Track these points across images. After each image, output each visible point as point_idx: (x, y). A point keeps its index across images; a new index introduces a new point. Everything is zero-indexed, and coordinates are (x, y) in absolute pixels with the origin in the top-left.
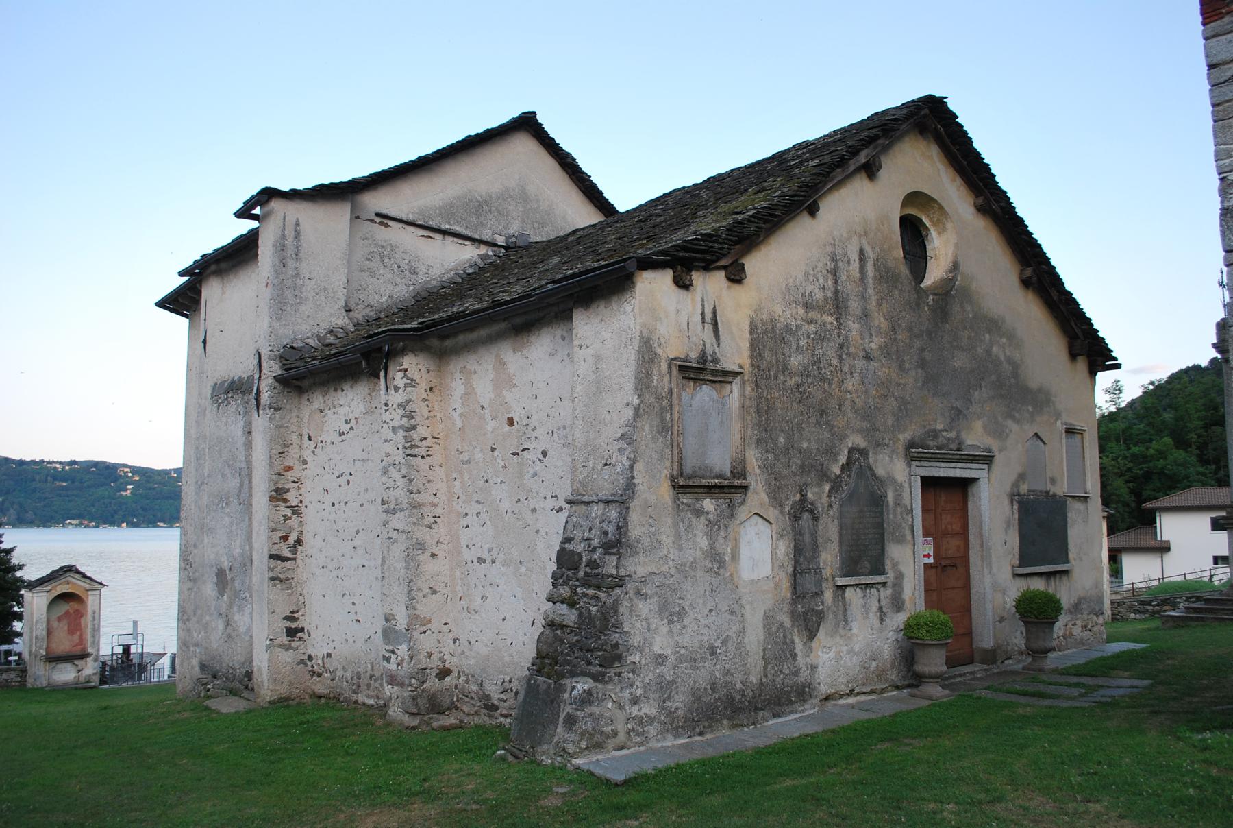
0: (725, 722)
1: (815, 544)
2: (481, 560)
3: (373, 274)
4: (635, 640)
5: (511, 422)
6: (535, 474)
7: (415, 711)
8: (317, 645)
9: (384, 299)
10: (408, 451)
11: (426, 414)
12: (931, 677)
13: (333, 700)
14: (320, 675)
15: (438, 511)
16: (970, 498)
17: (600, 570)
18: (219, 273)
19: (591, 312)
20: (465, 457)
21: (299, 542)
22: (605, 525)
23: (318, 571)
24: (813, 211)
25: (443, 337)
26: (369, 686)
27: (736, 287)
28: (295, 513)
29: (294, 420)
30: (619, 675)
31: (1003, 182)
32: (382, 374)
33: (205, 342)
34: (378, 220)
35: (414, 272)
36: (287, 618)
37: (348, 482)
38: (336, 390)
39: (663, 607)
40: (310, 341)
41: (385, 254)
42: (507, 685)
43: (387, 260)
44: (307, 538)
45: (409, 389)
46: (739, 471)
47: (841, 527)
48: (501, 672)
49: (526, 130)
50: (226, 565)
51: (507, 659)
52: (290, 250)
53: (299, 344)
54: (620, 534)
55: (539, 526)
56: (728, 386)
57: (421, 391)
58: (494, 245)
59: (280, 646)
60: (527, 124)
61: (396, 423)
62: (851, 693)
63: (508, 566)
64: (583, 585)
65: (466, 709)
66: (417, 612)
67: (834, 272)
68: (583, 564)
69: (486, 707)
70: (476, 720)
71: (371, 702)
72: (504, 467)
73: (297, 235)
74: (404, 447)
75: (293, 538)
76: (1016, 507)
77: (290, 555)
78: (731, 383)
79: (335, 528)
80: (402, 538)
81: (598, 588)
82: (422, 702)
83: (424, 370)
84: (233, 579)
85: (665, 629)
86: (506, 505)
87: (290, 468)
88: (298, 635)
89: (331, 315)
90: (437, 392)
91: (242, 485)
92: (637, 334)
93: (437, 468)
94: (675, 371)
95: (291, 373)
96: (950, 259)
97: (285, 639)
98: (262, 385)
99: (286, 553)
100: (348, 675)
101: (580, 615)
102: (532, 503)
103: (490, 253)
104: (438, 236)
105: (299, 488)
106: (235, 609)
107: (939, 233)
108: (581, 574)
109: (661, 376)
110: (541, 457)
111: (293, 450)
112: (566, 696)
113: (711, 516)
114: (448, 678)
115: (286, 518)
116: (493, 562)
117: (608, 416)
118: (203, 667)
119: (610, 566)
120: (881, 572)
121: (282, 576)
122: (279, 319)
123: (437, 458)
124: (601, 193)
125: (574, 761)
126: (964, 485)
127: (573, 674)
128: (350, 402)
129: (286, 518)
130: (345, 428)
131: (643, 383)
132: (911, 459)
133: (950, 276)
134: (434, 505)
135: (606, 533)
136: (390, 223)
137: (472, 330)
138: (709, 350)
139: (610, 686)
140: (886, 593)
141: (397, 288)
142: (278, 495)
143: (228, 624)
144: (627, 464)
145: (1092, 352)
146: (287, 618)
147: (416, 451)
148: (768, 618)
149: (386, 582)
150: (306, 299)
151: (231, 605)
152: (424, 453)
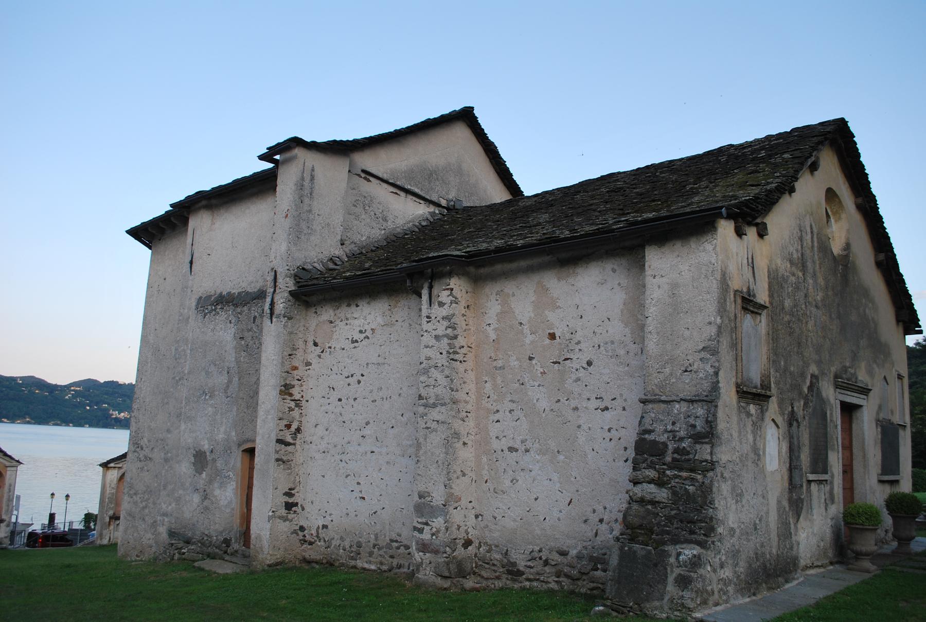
0: (764, 585)
1: (799, 447)
2: (511, 449)
3: (357, 217)
4: (720, 515)
5: (552, 336)
6: (578, 380)
7: (447, 574)
8: (312, 519)
9: (364, 238)
10: (452, 356)
11: (464, 327)
12: (867, 554)
13: (330, 565)
14: (311, 543)
15: (469, 407)
16: (855, 421)
17: (691, 456)
18: (210, 207)
19: (666, 249)
20: (500, 363)
21: (298, 430)
22: (691, 421)
23: (318, 456)
24: (792, 190)
25: (479, 266)
26: (371, 554)
27: (761, 240)
28: (297, 405)
29: (302, 329)
30: (713, 542)
31: (875, 189)
32: (425, 293)
33: (191, 263)
34: (363, 175)
35: (385, 220)
36: (286, 494)
37: (359, 382)
38: (349, 305)
39: (734, 488)
40: (316, 265)
41: (366, 202)
42: (536, 555)
43: (367, 208)
44: (308, 429)
45: (454, 305)
46: (766, 386)
47: (810, 434)
48: (530, 543)
49: (464, 121)
50: (206, 447)
51: (538, 532)
52: (306, 189)
53: (309, 267)
54: (711, 427)
55: (581, 422)
56: (758, 317)
57: (459, 309)
58: (438, 205)
59: (280, 517)
60: (467, 116)
61: (440, 332)
62: (812, 567)
63: (544, 454)
64: (670, 468)
65: (484, 573)
66: (452, 491)
67: (801, 239)
68: (670, 452)
69: (509, 572)
70: (499, 584)
71: (373, 567)
72: (543, 373)
73: (312, 178)
74: (448, 352)
75: (294, 426)
76: (879, 429)
77: (291, 441)
78: (760, 314)
79: (341, 419)
80: (441, 428)
81: (692, 470)
82: (453, 567)
83: (464, 290)
84: (214, 460)
85: (734, 507)
86: (544, 404)
87: (296, 368)
88: (294, 509)
89: (331, 245)
90: (472, 310)
91: (230, 381)
92: (719, 268)
93: (470, 372)
94: (739, 301)
95: (303, 290)
96: (843, 240)
97: (283, 512)
98: (277, 298)
99: (289, 439)
100: (347, 544)
101: (674, 493)
102: (573, 403)
103: (437, 212)
104: (402, 194)
105: (302, 385)
106: (216, 485)
107: (836, 221)
108: (668, 459)
109: (731, 303)
110: (585, 366)
111: (299, 354)
112: (672, 560)
113: (754, 418)
114: (470, 548)
115: (291, 409)
116: (527, 451)
117: (687, 333)
118: (172, 534)
119: (703, 452)
120: (825, 472)
121: (285, 458)
122: (295, 244)
123: (470, 364)
124: (511, 175)
125: (694, 615)
126: (859, 407)
127: (676, 541)
128: (369, 315)
129: (291, 409)
130: (357, 336)
131: (722, 310)
132: (837, 386)
133: (845, 253)
134: (467, 402)
135: (694, 426)
136: (371, 179)
137: (511, 261)
138: (751, 288)
139: (709, 552)
140: (828, 488)
141: (373, 231)
142: (286, 390)
143: (205, 497)
144: (711, 371)
145: (909, 320)
146: (286, 494)
147: (456, 357)
148: (779, 502)
149: (421, 465)
150: (315, 231)
151: (210, 482)
152: (461, 359)
